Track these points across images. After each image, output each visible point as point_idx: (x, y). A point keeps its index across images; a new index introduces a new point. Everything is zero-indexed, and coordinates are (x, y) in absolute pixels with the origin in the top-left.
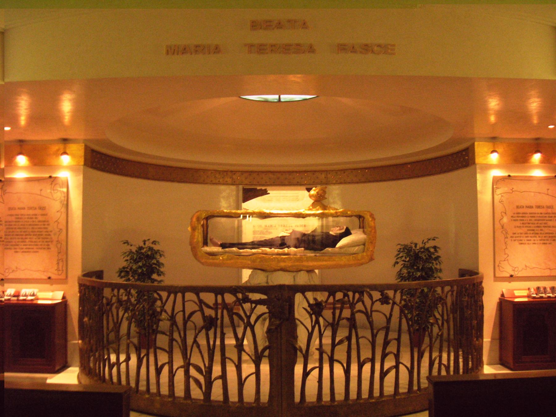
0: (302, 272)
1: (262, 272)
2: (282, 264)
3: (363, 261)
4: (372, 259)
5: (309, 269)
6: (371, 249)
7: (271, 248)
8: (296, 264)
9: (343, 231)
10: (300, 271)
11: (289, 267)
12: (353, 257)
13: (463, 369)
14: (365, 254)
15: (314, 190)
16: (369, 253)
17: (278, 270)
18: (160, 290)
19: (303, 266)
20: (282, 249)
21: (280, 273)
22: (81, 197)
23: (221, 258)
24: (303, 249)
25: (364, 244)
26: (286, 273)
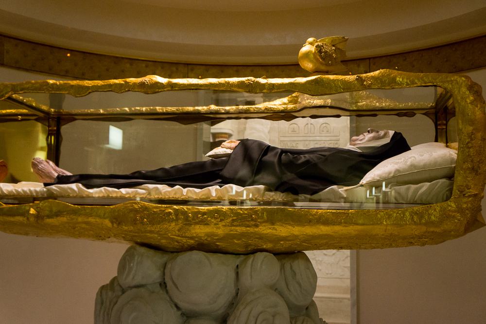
0: (260, 256)
1: (151, 252)
2: (200, 231)
3: (447, 226)
4: (474, 223)
5: (283, 246)
6: (474, 191)
7: (172, 186)
8: (240, 229)
9: (387, 140)
10: (254, 252)
11: (221, 239)
12: (413, 213)
13: (176, 84)
14: (452, 205)
15: (311, 44)
16: (466, 203)
17: (191, 248)
18: (304, 250)
19: (261, 237)
20: (201, 188)
21: (197, 255)
22: (60, 151)
23: (32, 211)
24: (262, 187)
25: (450, 177)
26: (214, 258)
